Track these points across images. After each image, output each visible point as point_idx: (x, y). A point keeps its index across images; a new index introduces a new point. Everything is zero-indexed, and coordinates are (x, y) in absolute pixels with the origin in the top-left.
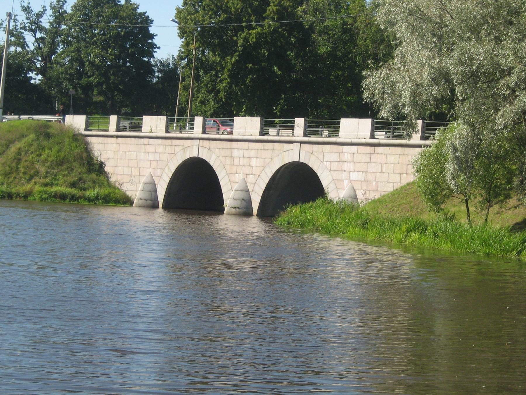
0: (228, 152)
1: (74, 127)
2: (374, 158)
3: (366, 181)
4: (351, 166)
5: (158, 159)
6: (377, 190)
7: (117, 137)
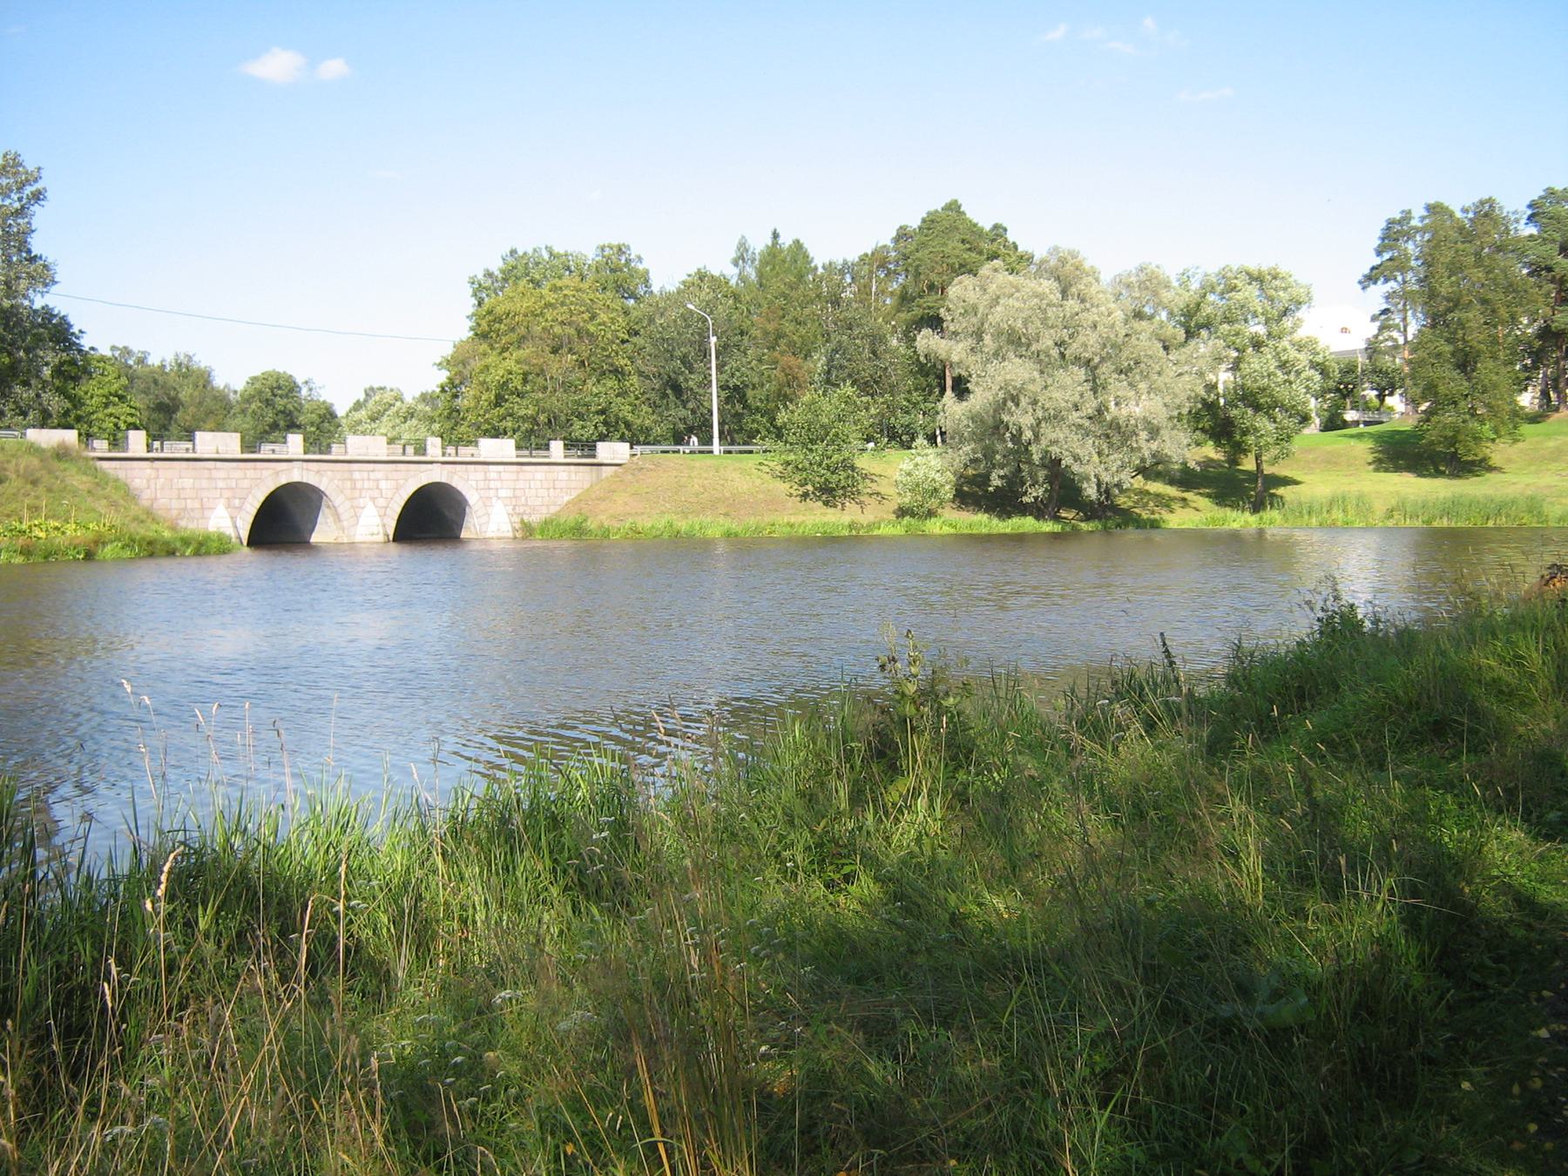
0: (346, 475)
1: (55, 446)
2: (521, 476)
3: (515, 497)
4: (498, 484)
5: (234, 486)
6: (527, 505)
7: (701, 452)
